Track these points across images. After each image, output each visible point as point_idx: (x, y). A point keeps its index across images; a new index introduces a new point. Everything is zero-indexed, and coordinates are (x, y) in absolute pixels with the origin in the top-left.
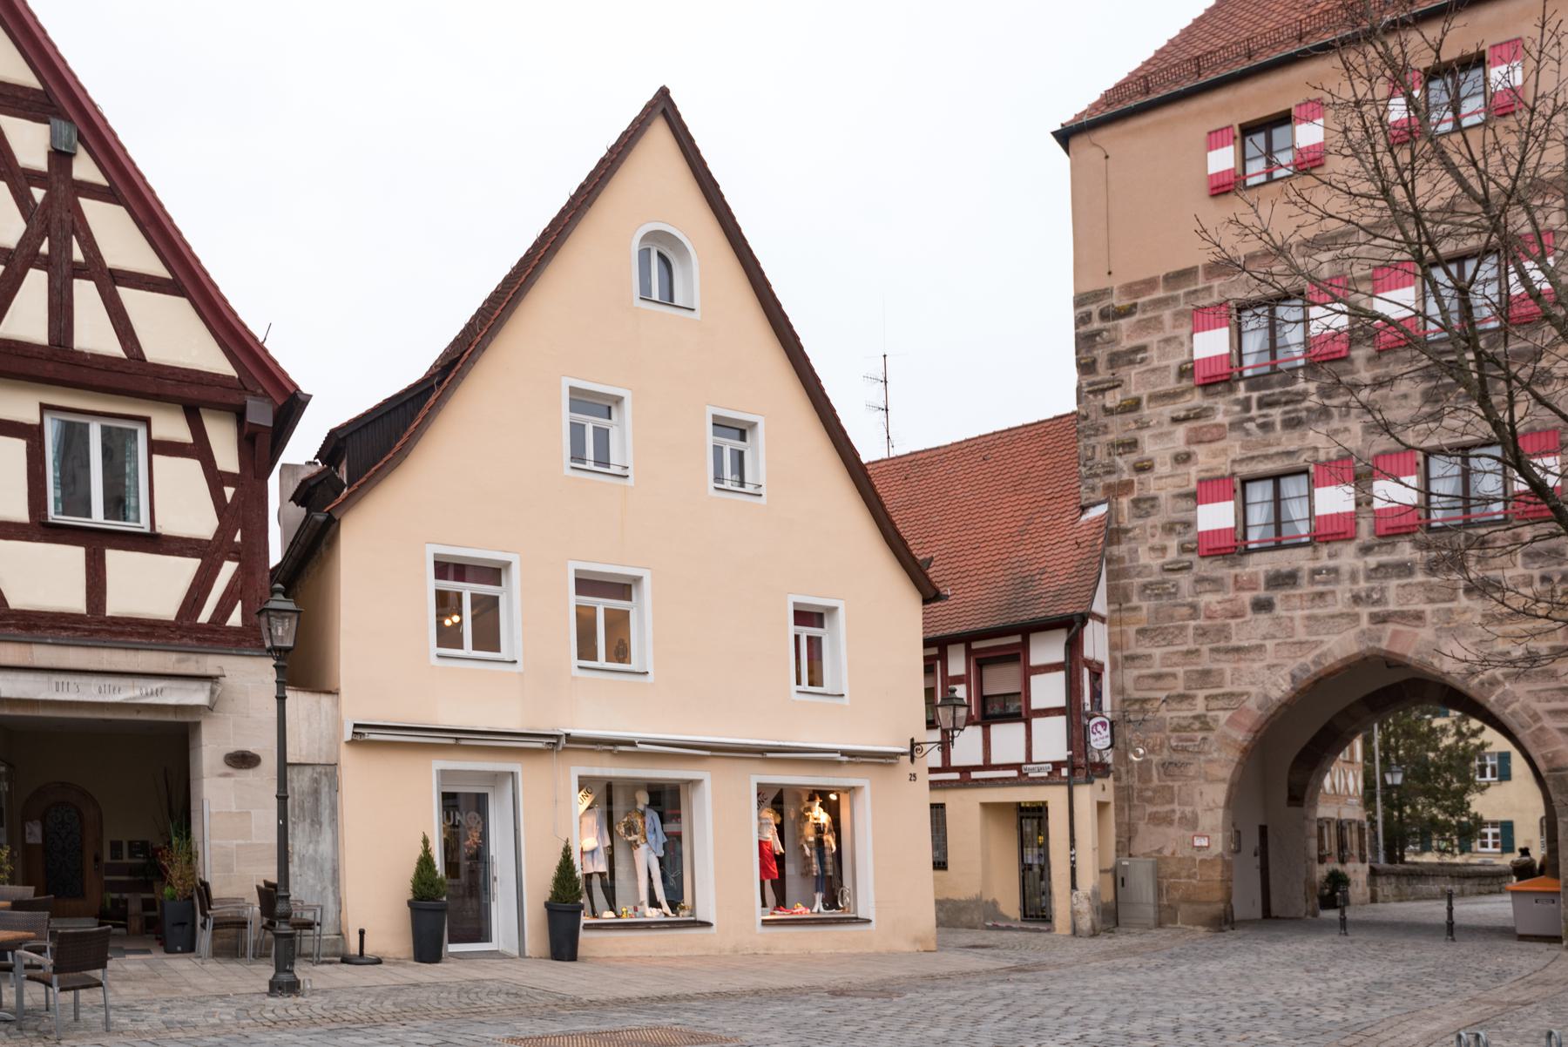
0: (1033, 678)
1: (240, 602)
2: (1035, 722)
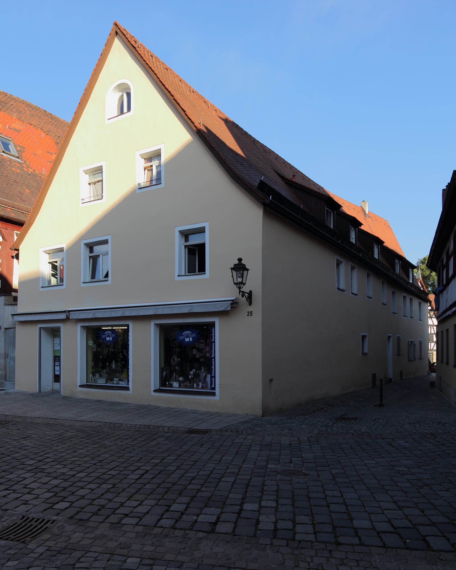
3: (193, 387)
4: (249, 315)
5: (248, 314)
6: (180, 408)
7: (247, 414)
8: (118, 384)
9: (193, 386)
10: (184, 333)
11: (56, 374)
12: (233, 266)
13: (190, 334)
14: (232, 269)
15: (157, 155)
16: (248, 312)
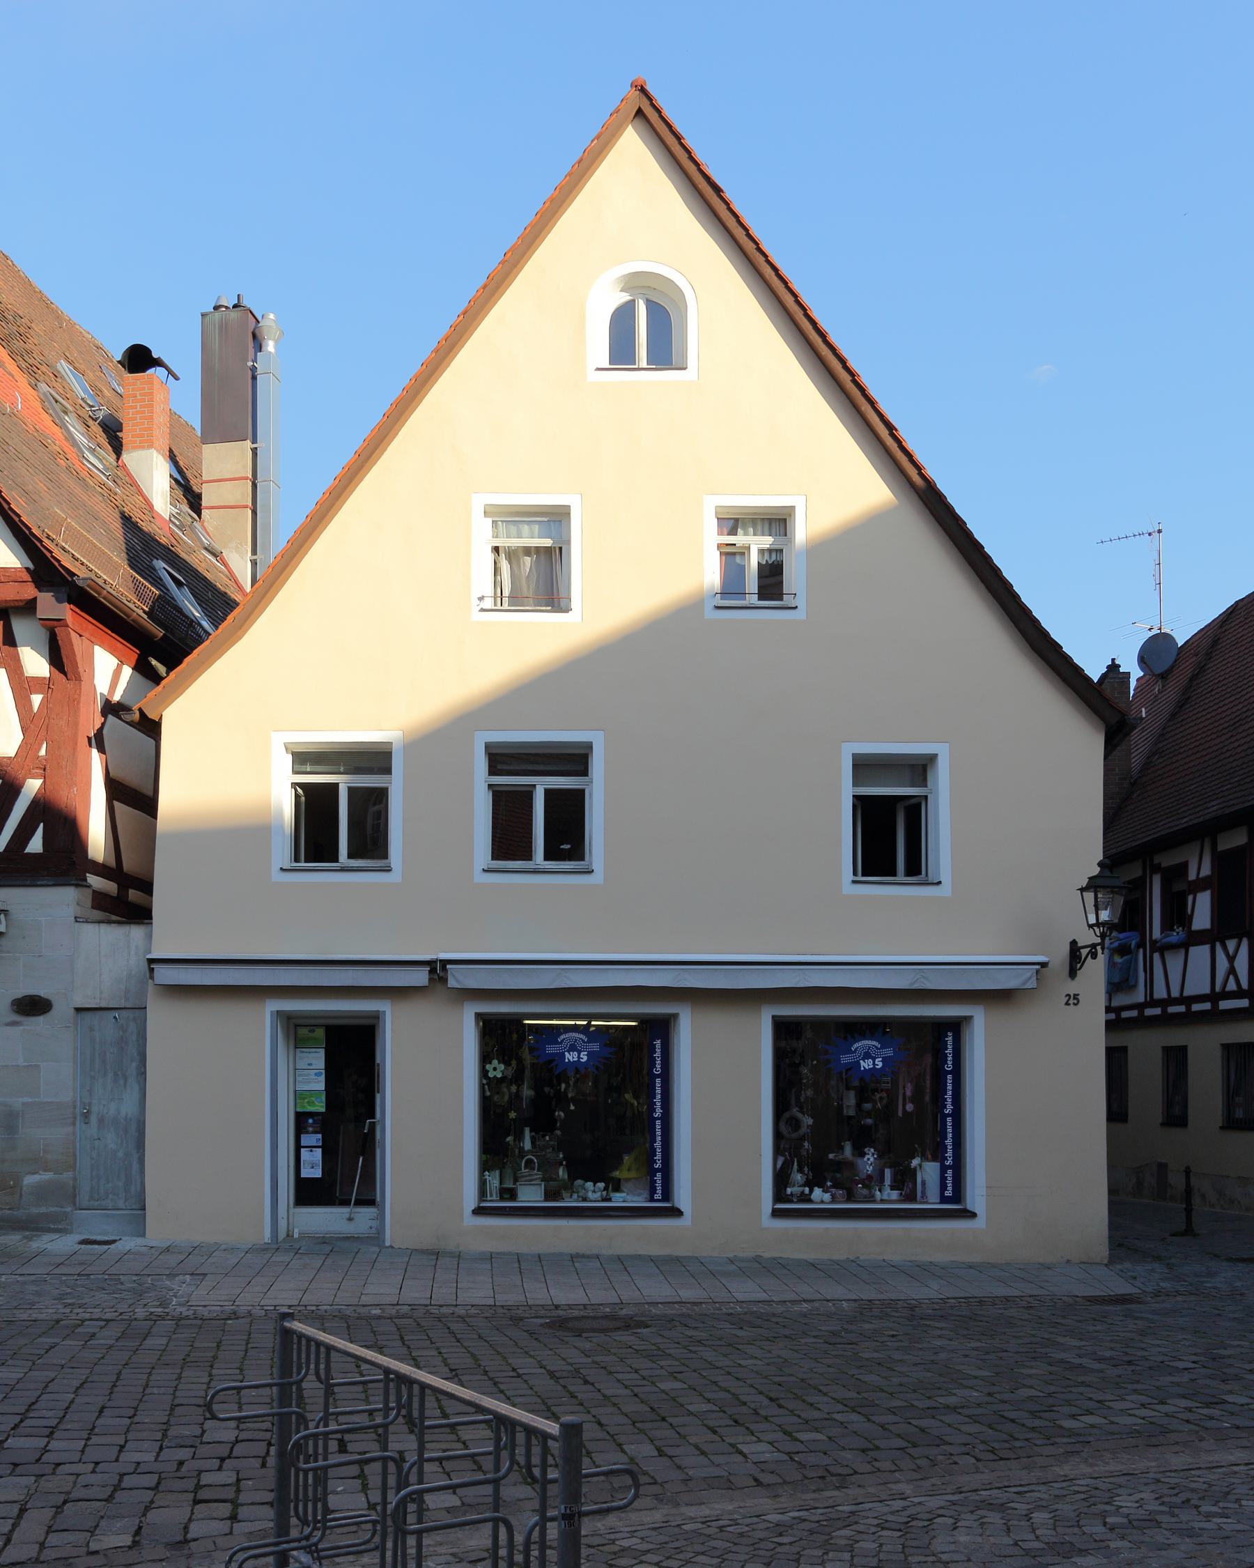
0: (548, 1486)
1: (42, 824)
2: (1207, 990)
3: (871, 1199)
4: (1069, 1004)
5: (1068, 1000)
6: (861, 1258)
7: (1068, 1261)
8: (609, 1200)
9: (873, 1196)
10: (856, 1046)
11: (303, 1175)
12: (1084, 883)
13: (582, 1040)
14: (1082, 890)
15: (778, 522)
16: (1068, 995)
